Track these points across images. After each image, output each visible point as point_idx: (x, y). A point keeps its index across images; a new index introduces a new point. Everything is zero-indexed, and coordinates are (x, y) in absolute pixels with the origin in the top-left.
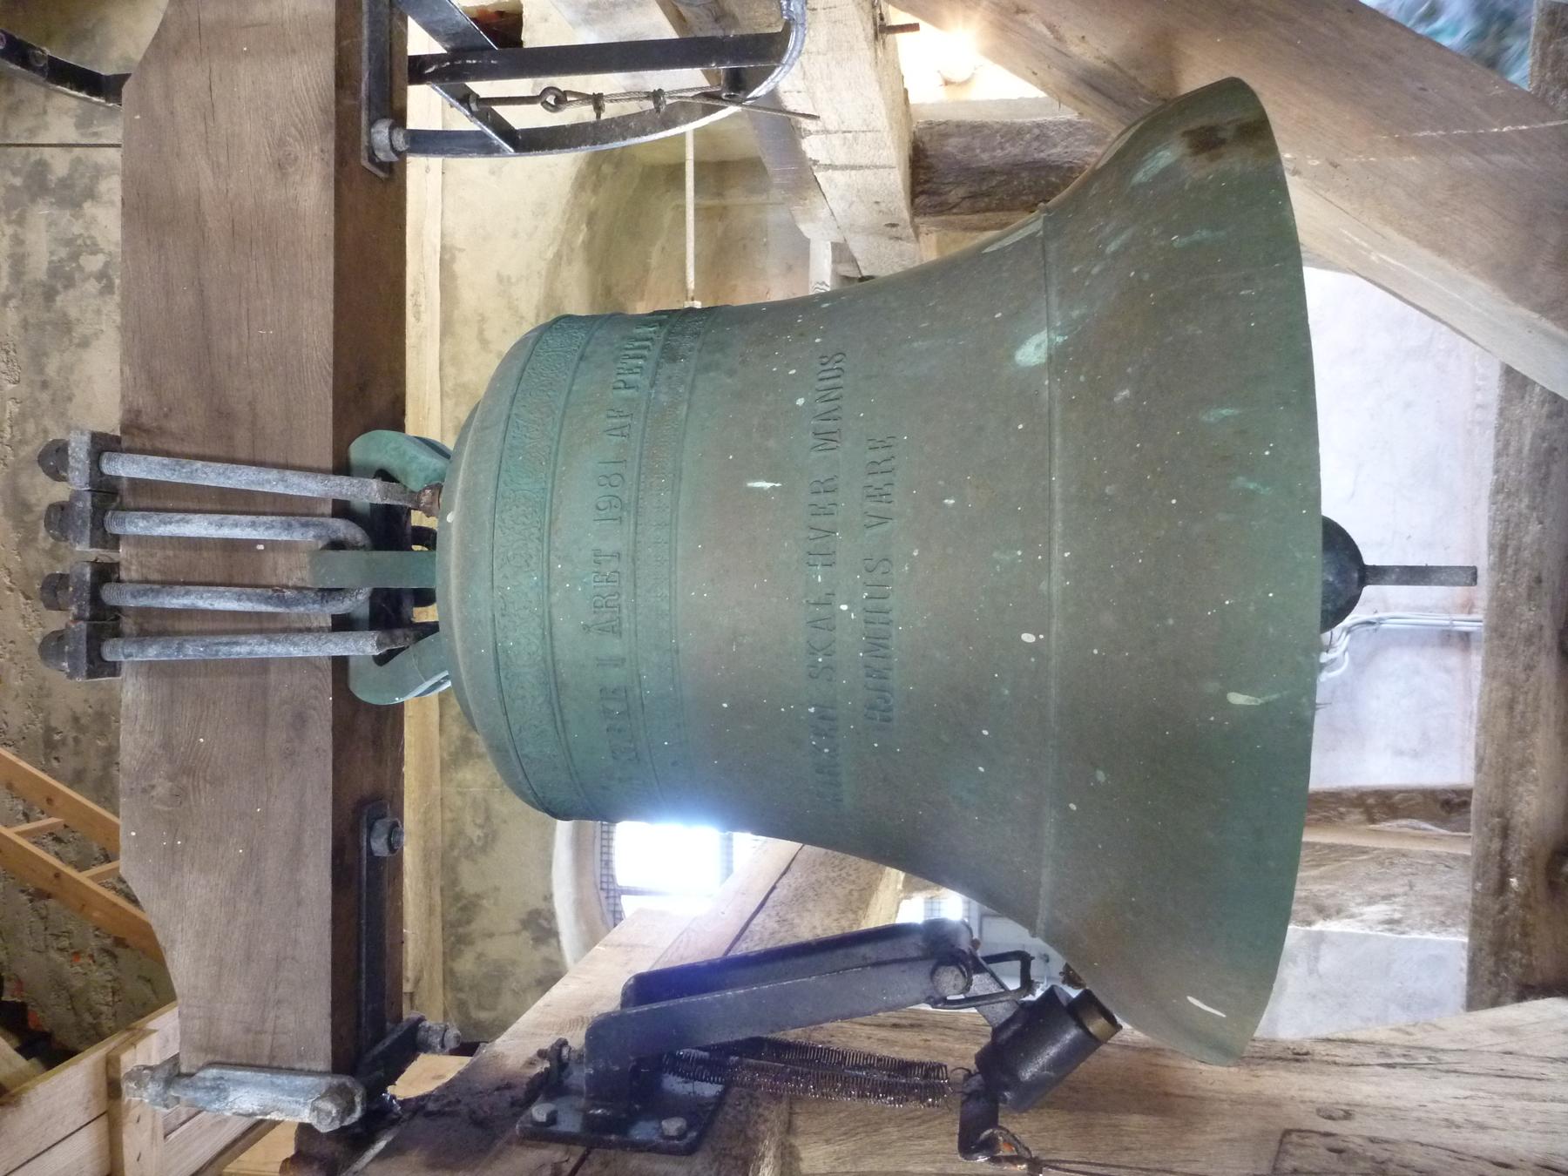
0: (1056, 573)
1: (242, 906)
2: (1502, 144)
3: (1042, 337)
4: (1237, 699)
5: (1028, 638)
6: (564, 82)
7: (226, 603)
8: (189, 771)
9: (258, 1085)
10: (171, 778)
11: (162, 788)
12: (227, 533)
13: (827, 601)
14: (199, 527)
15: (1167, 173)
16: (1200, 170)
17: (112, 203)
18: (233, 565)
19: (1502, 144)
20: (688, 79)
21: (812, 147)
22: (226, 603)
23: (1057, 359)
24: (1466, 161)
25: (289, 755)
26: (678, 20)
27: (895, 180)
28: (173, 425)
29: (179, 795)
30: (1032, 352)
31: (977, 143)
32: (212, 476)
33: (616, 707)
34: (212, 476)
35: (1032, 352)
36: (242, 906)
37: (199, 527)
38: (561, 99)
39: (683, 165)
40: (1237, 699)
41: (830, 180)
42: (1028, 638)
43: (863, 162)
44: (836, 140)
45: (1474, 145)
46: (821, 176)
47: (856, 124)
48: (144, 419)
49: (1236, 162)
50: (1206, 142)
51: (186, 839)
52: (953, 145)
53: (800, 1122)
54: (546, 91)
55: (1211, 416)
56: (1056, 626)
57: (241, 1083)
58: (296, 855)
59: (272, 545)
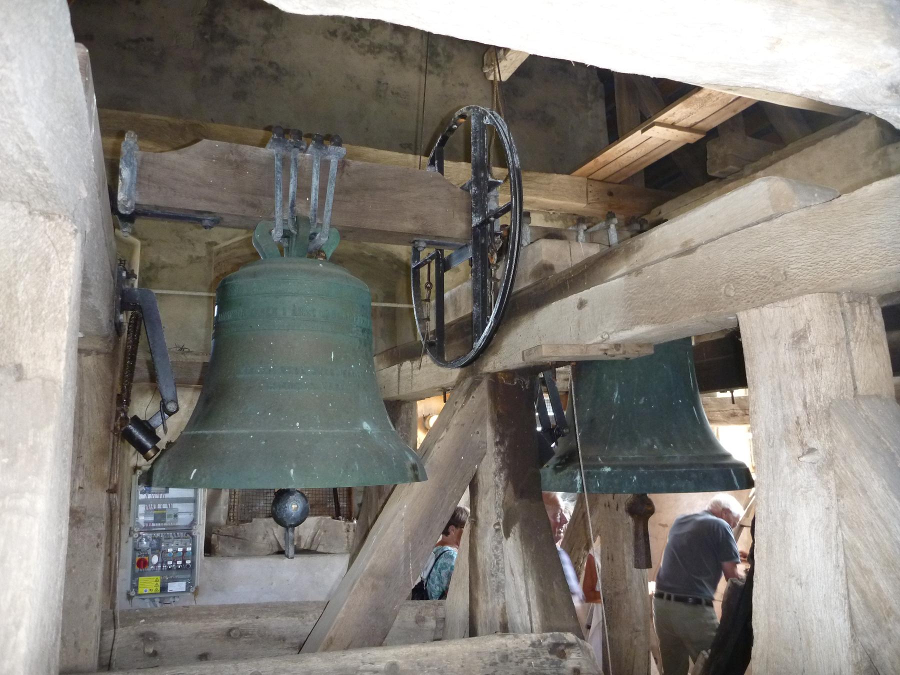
0: (315, 431)
1: (193, 180)
2: (407, 567)
3: (369, 428)
4: (292, 471)
5: (298, 424)
6: (434, 289)
7: (292, 188)
8: (237, 167)
9: (132, 178)
10: (236, 161)
11: (233, 157)
12: (313, 191)
13: (303, 373)
14: (315, 182)
15: (407, 458)
16: (408, 466)
17: (392, 38)
18: (304, 190)
19: (407, 567)
20: (432, 325)
21: (407, 364)
22: (292, 188)
23: (365, 432)
24: (402, 557)
25: (243, 201)
26: (450, 325)
27: (393, 394)
28: (344, 176)
29: (230, 163)
30: (366, 426)
31: (404, 425)
32: (331, 189)
33: (271, 312)
34: (331, 189)
35: (366, 426)
36: (193, 180)
37: (315, 182)
38: (429, 289)
39: (395, 302)
40: (292, 471)
41: (394, 370)
42: (298, 424)
43: (401, 383)
44: (409, 373)
45: (407, 560)
46: (396, 366)
47: (414, 381)
48: (347, 167)
49: (410, 473)
50: (414, 468)
51: (215, 163)
52: (236, 551)
53: (102, 356)
54: (431, 284)
55: (356, 465)
56: (302, 431)
57: (132, 172)
58: (210, 200)
59: (309, 203)
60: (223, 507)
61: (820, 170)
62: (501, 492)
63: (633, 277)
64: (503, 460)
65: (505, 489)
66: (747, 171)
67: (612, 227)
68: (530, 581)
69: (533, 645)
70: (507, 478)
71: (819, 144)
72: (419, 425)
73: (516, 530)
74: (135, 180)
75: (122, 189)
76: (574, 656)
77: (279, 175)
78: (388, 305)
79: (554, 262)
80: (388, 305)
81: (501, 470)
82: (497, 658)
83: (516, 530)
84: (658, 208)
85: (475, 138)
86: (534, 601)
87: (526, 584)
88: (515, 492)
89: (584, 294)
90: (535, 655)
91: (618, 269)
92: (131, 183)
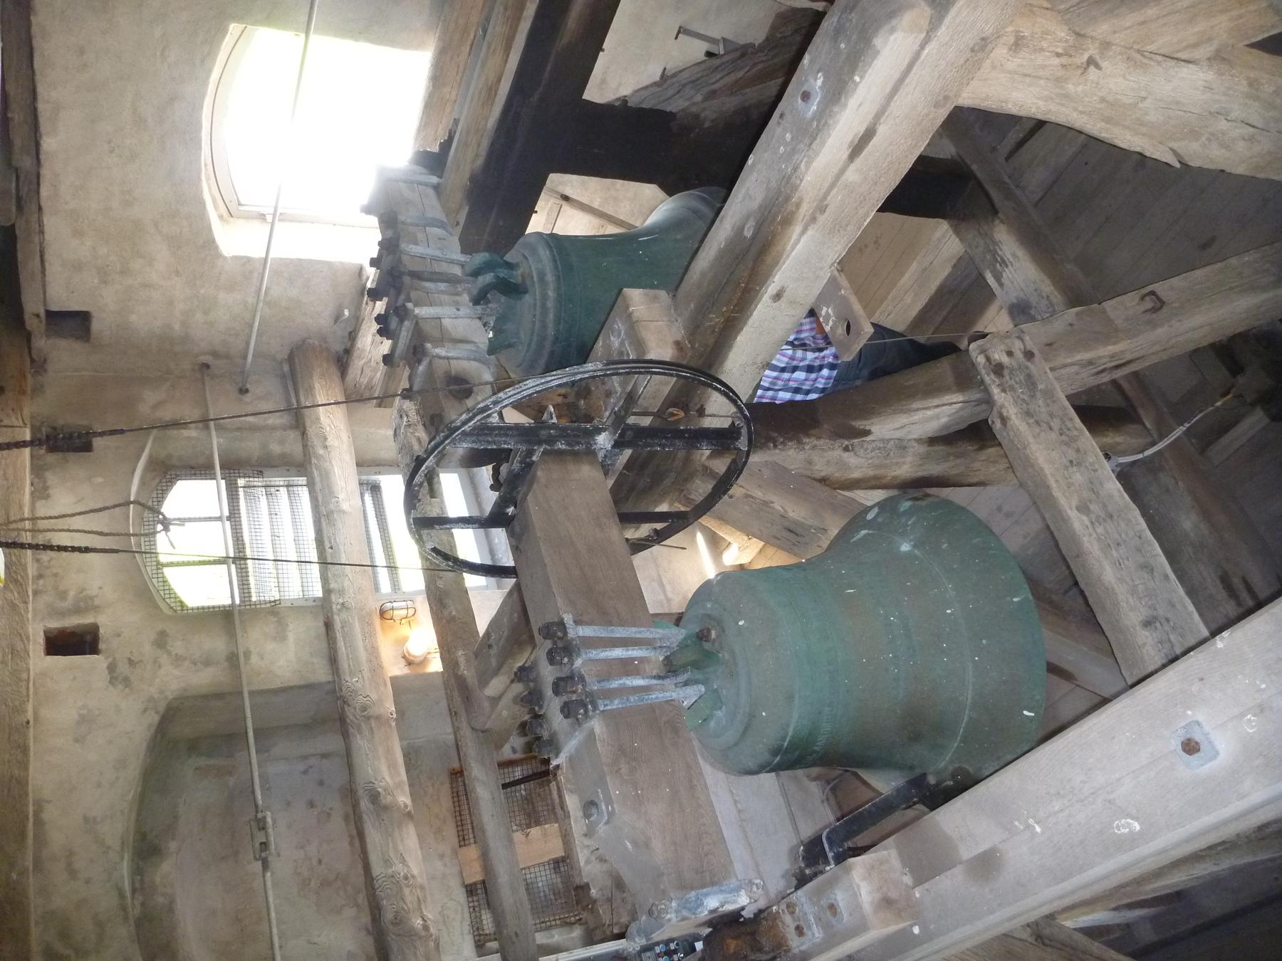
9: (715, 893)
14: (618, 653)
18: (627, 667)
37: (618, 653)
57: (706, 895)
60: (557, 937)
61: (82, 51)
62: (822, 442)
63: (821, 219)
64: (791, 439)
65: (819, 438)
66: (26, 163)
67: (417, 311)
68: (914, 406)
69: (1004, 391)
70: (808, 436)
71: (36, 43)
72: (421, 671)
73: (860, 424)
74: (715, 888)
75: (735, 902)
76: (997, 356)
77: (632, 699)
78: (251, 734)
79: (670, 340)
80: (251, 734)
81: (800, 442)
82: (1031, 421)
83: (860, 424)
84: (27, 316)
85: (489, 442)
86: (936, 401)
87: (918, 410)
88: (814, 428)
89: (772, 289)
90: (1012, 389)
91: (790, 238)
92: (721, 891)
